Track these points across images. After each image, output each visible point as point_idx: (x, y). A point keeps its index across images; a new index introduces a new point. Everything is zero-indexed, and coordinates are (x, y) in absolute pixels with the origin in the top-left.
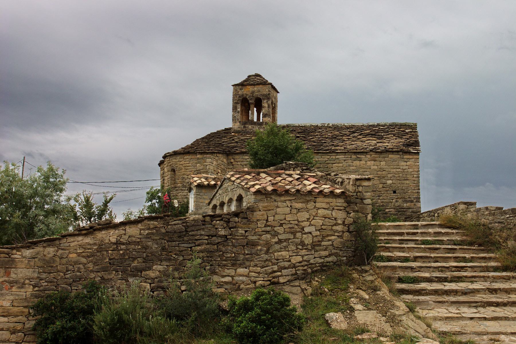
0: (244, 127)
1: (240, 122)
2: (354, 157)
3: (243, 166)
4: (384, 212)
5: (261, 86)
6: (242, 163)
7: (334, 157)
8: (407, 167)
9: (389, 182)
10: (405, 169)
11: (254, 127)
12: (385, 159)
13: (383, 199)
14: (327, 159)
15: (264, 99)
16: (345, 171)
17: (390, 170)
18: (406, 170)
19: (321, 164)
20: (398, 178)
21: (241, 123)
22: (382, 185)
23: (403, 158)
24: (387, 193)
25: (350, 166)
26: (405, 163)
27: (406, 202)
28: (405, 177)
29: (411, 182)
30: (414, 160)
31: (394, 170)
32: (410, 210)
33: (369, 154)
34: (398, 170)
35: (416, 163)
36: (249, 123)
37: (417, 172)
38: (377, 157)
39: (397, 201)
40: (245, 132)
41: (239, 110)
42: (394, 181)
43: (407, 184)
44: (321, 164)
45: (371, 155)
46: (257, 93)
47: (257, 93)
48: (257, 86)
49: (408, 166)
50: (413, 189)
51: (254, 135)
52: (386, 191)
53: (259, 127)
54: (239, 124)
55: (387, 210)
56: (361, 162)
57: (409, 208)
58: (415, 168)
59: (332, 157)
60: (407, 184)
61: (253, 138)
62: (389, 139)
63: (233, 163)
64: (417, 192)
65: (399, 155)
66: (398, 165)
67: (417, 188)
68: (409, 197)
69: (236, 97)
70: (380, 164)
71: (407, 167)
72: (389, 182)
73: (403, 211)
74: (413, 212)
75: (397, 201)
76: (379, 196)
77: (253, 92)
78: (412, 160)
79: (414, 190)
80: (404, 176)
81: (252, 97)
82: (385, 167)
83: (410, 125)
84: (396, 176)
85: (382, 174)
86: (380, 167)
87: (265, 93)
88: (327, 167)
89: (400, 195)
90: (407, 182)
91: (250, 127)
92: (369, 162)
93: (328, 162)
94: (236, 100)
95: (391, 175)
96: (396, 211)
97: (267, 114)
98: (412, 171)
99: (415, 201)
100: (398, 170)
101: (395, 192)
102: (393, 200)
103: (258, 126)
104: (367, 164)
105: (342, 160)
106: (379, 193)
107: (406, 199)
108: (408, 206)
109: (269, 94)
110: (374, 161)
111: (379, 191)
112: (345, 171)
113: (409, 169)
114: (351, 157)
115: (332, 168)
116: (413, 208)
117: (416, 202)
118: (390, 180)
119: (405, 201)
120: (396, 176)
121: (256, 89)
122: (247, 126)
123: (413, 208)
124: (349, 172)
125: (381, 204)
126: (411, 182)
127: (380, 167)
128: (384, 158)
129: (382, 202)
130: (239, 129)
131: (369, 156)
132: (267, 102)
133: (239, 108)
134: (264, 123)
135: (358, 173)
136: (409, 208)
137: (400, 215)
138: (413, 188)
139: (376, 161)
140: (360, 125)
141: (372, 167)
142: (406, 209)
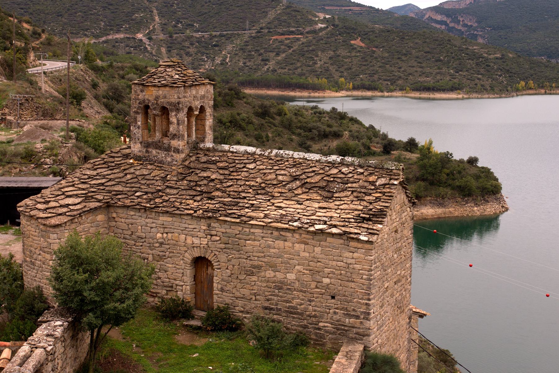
0: (147, 152)
1: (141, 143)
2: (276, 233)
3: (128, 225)
4: (317, 326)
5: (167, 89)
6: (127, 221)
7: (247, 230)
8: (353, 261)
9: (326, 281)
10: (350, 264)
11: (159, 153)
12: (322, 243)
13: (316, 306)
14: (238, 232)
15: (172, 111)
16: (263, 255)
17: (327, 261)
18: (351, 266)
19: (230, 237)
20: (339, 277)
21: (143, 144)
22: (316, 283)
23: (348, 246)
24: (322, 298)
25: (269, 247)
26: (351, 254)
27: (350, 316)
28: (349, 276)
29: (358, 286)
30: (364, 251)
31: (334, 263)
32: (355, 330)
33: (298, 232)
34: (340, 264)
35: (367, 256)
36: (153, 146)
37: (368, 271)
38: (309, 239)
39: (335, 313)
40: (147, 159)
41: (139, 123)
42: (332, 280)
43: (351, 288)
44: (230, 237)
45: (301, 234)
46: (162, 100)
47: (162, 100)
48: (163, 89)
49: (356, 259)
50: (360, 298)
51: (158, 166)
52: (320, 294)
53: (166, 154)
54: (139, 145)
55: (321, 324)
56: (285, 242)
57: (353, 327)
58: (366, 264)
59: (245, 229)
60: (351, 288)
61: (156, 173)
62: (341, 200)
63: (116, 219)
64: (366, 304)
65: (342, 239)
66: (341, 256)
67: (367, 297)
68: (354, 310)
69: (135, 102)
70: (314, 251)
71: (353, 261)
72: (326, 281)
73: (344, 330)
74: (357, 333)
75: (335, 313)
76: (310, 301)
77: (157, 98)
78: (362, 250)
79: (362, 299)
80: (349, 274)
81: (156, 106)
82: (321, 256)
83: (389, 169)
84: (336, 272)
85: (316, 267)
86: (312, 255)
87: (173, 100)
88: (239, 245)
89: (341, 304)
90: (353, 285)
91: (154, 152)
92: (297, 245)
93: (240, 236)
94: (135, 108)
95: (329, 270)
96: (334, 328)
97: (175, 135)
98: (361, 269)
99: (362, 317)
100: (340, 264)
101: (333, 297)
102: (330, 309)
103: (165, 153)
104: (295, 248)
105: (259, 236)
106: (310, 295)
107: (350, 311)
108: (352, 324)
109: (178, 103)
110: (305, 244)
111: (310, 293)
112: (263, 255)
113: (356, 264)
114: (272, 233)
115: (245, 246)
116: (359, 328)
117: (364, 318)
118: (327, 277)
119: (347, 314)
120: (336, 272)
121: (161, 92)
122: (150, 150)
123: (359, 328)
124: (268, 256)
125: (313, 313)
126: (358, 286)
127: (312, 255)
128: (320, 241)
129: (315, 311)
130: (140, 154)
131: (297, 236)
132: (176, 115)
133: (139, 121)
134: (173, 149)
135: (280, 259)
136: (353, 327)
137: (339, 334)
138: (361, 296)
139: (308, 244)
140: (315, 159)
141: (303, 254)
142: (349, 327)
